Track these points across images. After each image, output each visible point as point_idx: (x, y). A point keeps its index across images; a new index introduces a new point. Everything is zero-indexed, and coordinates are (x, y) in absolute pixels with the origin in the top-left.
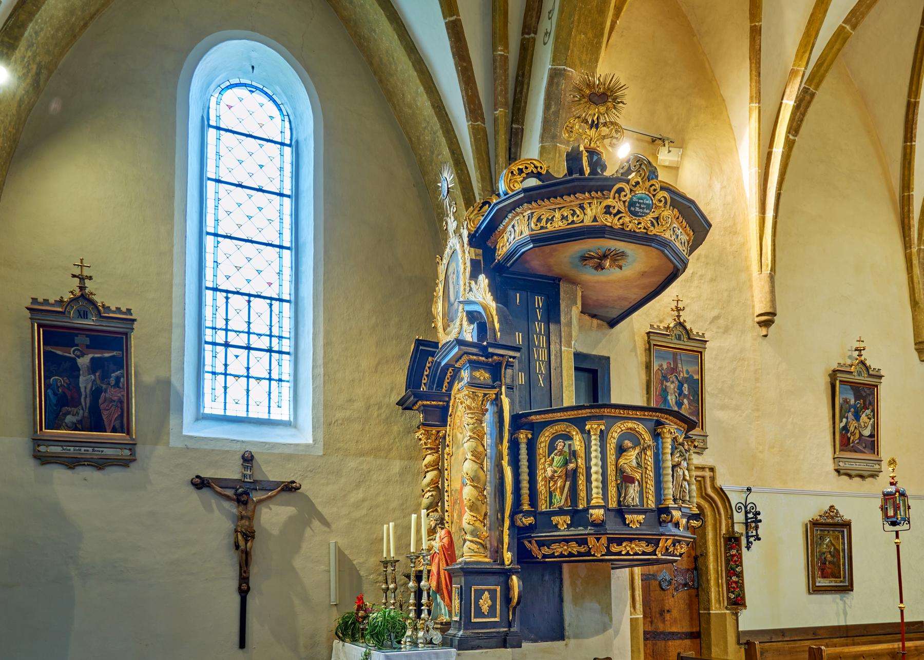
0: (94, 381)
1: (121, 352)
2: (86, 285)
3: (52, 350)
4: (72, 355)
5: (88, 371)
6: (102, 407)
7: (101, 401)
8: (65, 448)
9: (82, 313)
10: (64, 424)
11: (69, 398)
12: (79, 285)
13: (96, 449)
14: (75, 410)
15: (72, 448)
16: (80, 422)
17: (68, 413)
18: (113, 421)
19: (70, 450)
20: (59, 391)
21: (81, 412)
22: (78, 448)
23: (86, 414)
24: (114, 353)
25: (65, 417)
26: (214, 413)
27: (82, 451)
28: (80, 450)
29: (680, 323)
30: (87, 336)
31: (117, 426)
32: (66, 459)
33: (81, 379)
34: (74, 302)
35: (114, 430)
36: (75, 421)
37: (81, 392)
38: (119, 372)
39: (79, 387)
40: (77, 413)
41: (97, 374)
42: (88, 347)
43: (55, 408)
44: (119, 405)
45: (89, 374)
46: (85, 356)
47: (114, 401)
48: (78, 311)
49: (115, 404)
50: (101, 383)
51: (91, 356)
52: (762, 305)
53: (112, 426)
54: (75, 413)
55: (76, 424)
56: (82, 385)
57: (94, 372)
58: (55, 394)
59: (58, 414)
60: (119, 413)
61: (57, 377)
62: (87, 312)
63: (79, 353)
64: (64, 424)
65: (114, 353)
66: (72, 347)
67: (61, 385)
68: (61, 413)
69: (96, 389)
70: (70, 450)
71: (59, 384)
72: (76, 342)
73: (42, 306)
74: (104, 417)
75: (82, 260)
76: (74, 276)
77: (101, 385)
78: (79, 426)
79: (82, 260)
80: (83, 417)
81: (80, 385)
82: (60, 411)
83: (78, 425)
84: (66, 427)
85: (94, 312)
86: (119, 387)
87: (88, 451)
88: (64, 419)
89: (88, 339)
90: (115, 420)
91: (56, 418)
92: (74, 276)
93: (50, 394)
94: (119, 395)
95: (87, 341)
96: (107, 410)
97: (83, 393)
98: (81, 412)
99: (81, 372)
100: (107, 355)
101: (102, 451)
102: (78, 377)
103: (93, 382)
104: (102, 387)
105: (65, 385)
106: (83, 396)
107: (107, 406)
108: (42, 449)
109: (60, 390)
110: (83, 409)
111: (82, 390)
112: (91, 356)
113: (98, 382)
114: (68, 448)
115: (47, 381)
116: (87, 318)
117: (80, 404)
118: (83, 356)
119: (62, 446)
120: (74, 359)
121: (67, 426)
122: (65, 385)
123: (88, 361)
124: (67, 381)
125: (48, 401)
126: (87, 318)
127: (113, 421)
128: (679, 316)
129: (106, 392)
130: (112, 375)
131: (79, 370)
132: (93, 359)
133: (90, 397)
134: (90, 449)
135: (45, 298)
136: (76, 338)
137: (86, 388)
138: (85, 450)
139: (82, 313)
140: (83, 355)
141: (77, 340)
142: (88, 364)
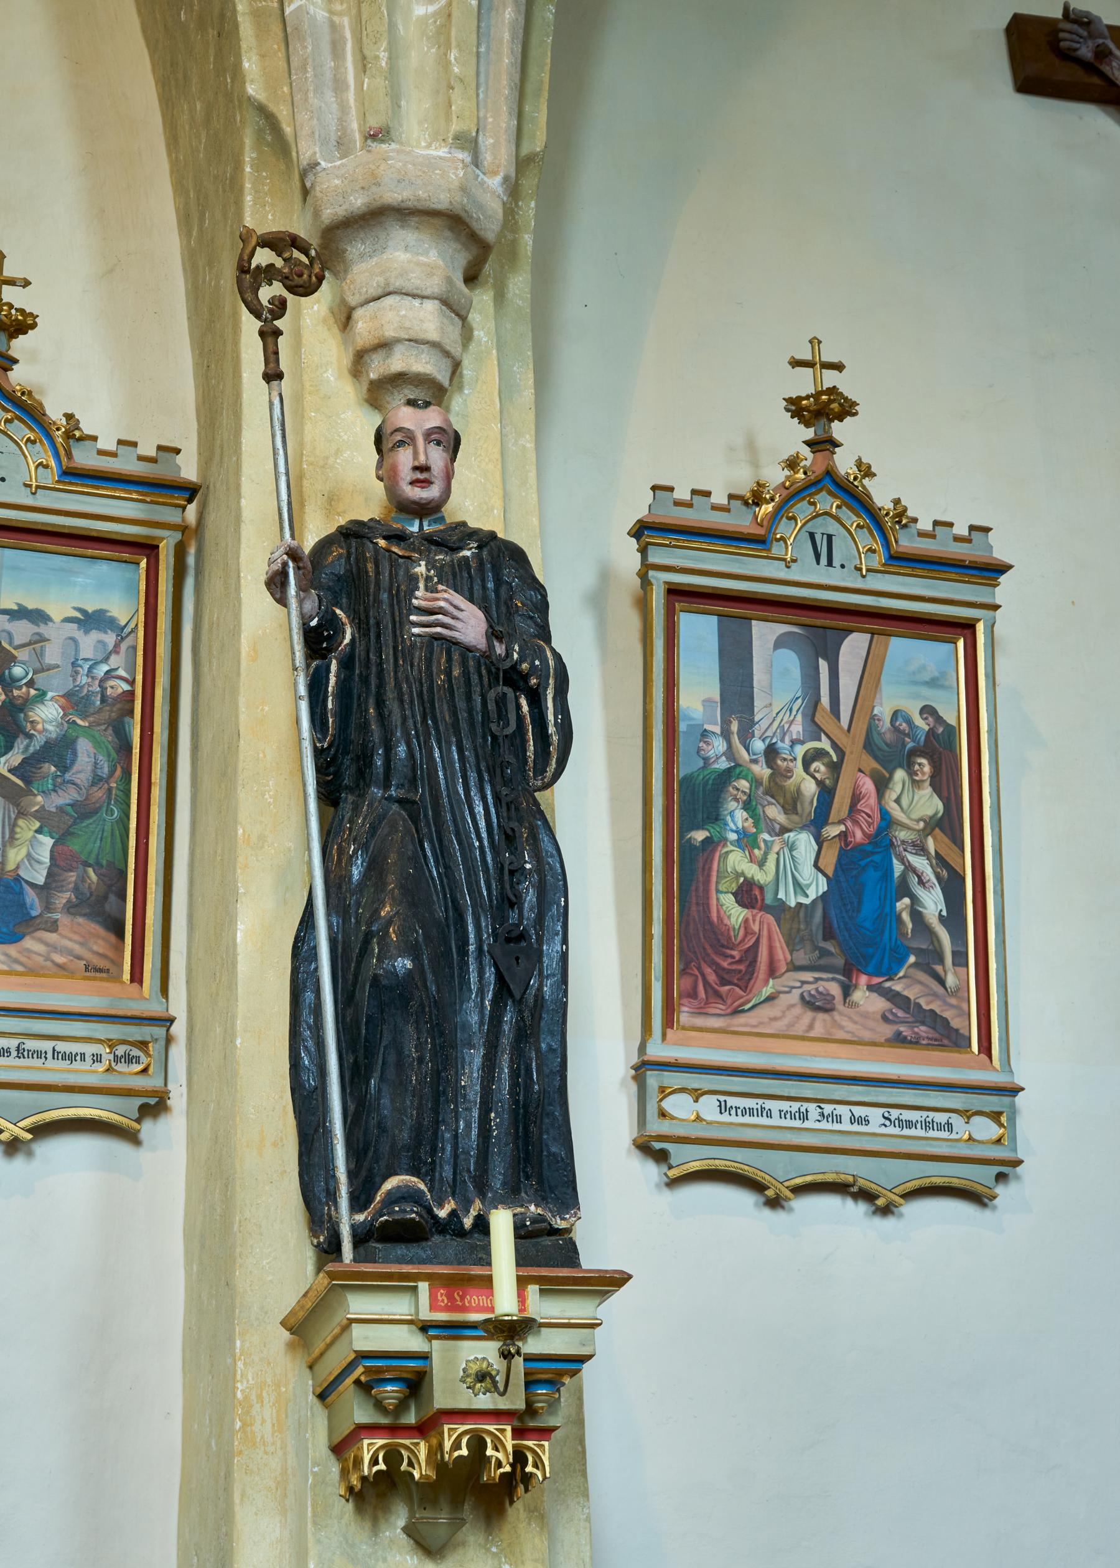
22: (795, 1106)
62: (830, 538)
79: (815, 342)
87: (864, 1121)
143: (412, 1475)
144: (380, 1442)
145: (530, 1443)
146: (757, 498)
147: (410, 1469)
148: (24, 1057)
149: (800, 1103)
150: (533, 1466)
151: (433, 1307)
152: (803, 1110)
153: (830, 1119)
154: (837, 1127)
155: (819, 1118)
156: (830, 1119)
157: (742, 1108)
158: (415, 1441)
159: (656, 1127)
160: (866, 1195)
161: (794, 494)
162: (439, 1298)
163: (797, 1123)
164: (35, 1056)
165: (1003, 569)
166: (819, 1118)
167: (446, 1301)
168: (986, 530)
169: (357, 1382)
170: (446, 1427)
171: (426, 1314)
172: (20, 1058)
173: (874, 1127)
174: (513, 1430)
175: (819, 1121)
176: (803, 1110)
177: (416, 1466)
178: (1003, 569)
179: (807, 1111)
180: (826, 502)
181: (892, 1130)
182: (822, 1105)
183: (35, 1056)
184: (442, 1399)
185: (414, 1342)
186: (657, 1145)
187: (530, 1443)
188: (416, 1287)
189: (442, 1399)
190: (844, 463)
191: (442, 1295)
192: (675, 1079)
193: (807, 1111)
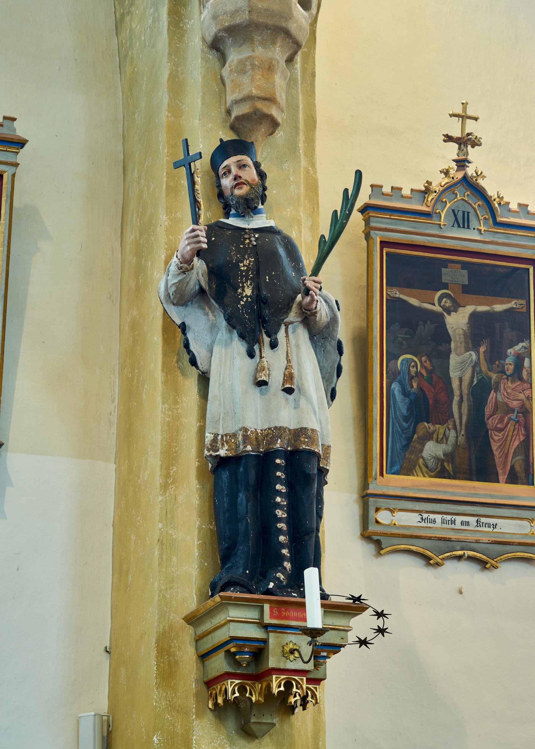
0: (477, 364)
1: (523, 302)
2: (470, 158)
3: (402, 296)
4: (437, 308)
5: (466, 343)
6: (491, 423)
7: (488, 410)
8: (425, 516)
9: (460, 216)
10: (421, 461)
11: (431, 401)
12: (456, 157)
13: (483, 520)
14: (440, 429)
15: (438, 517)
16: (450, 456)
17: (429, 436)
18: (510, 458)
19: (434, 521)
20: (412, 387)
21: (452, 433)
22: (449, 517)
23: (461, 439)
24: (512, 304)
25: (424, 445)
26: (466, 414)
27: (458, 526)
28: (453, 522)
29: (465, 178)
30: (465, 265)
31: (518, 468)
32: (429, 543)
33: (454, 359)
34: (447, 194)
35: (513, 479)
36: (440, 454)
37: (452, 390)
38: (521, 345)
39: (450, 378)
40: (446, 437)
41: (482, 349)
42: (466, 290)
43: (405, 425)
44: (522, 419)
45: (467, 350)
46: (461, 309)
47: (513, 411)
48: (453, 211)
49: (513, 416)
50: (490, 370)
51: (470, 309)
52: (220, 120)
53: (509, 468)
54: (441, 436)
55: (442, 461)
56: (454, 374)
57: (475, 347)
58: (405, 393)
59: (410, 439)
60: (522, 438)
61: (409, 356)
62: (468, 213)
63: (448, 303)
64: (421, 461)
65: (512, 304)
66: (438, 290)
67: (416, 372)
68: (416, 436)
69: (479, 381)
70: (434, 521)
71: (413, 370)
72: (445, 279)
73: (391, 201)
74: (494, 447)
75: (465, 105)
76: (449, 138)
77: (489, 373)
78: (449, 467)
79: (465, 105)
80: (456, 445)
81: (452, 374)
82: (414, 432)
83: (446, 464)
84: (424, 469)
85: (483, 214)
86: (521, 379)
87: (468, 524)
88: (421, 451)
89: (465, 272)
90: (515, 454)
91: (406, 447)
92: (449, 138)
93: (396, 393)
94: (522, 396)
95: (463, 277)
96: (500, 430)
97: (457, 392)
98: (452, 434)
99: (453, 345)
100: (499, 308)
101: (495, 526)
102: (448, 353)
103: (474, 367)
104: (490, 379)
105: (424, 372)
106: (456, 399)
107: (501, 421)
108: (384, 517)
109: (415, 385)
110: (455, 428)
111: (455, 384)
112: (470, 309)
113: (484, 366)
114: (432, 516)
115: (392, 363)
116: (468, 228)
117: (452, 416)
118: (456, 311)
119: (420, 512)
120: (441, 316)
121: (427, 467)
122: (424, 372)
123: (465, 320)
124: (428, 364)
125: (392, 409)
126: (468, 228)
127: (510, 458)
128: (462, 163)
129: (497, 389)
130: (509, 351)
131: (448, 340)
132: (474, 316)
133: (468, 400)
134: (472, 520)
135: (396, 185)
136: (444, 270)
137: (461, 380)
138: (462, 523)
139: (460, 216)
140: (456, 306)
141: (447, 275)
142: (465, 328)
143: (251, 700)
144: (237, 681)
145: (296, 678)
146: (427, 191)
147: (251, 697)
148: (480, 526)
149: (442, 516)
150: (235, 693)
151: (272, 616)
152: (453, 519)
153: (426, 521)
154: (453, 526)
155: (421, 521)
156: (426, 521)
157: (485, 523)
158: (315, 686)
159: (373, 528)
160: (427, 559)
161: (449, 188)
162: (274, 611)
163: (450, 526)
164: (487, 526)
165: (21, 143)
166: (421, 521)
167: (277, 613)
168: (14, 119)
169: (228, 652)
170: (274, 676)
171: (267, 620)
172: (478, 526)
173: (438, 524)
174: (307, 679)
175: (420, 522)
176: (453, 519)
177: (254, 696)
178: (21, 143)
179: (455, 520)
180: (462, 194)
181: (423, 524)
182: (422, 514)
183: (487, 526)
184: (273, 662)
185: (254, 632)
186: (375, 538)
187: (296, 678)
188: (263, 606)
189: (273, 662)
190: (470, 171)
191: (275, 611)
192: (382, 502)
193: (455, 520)
